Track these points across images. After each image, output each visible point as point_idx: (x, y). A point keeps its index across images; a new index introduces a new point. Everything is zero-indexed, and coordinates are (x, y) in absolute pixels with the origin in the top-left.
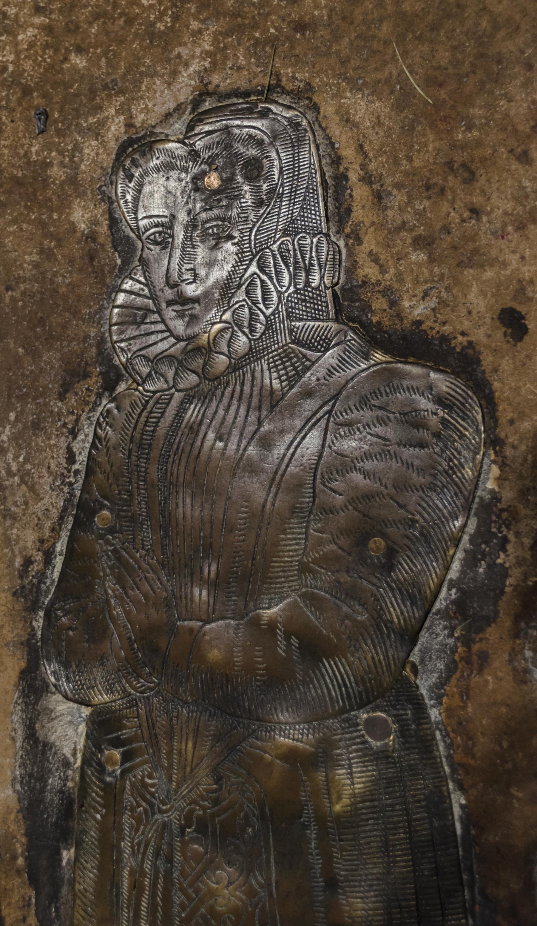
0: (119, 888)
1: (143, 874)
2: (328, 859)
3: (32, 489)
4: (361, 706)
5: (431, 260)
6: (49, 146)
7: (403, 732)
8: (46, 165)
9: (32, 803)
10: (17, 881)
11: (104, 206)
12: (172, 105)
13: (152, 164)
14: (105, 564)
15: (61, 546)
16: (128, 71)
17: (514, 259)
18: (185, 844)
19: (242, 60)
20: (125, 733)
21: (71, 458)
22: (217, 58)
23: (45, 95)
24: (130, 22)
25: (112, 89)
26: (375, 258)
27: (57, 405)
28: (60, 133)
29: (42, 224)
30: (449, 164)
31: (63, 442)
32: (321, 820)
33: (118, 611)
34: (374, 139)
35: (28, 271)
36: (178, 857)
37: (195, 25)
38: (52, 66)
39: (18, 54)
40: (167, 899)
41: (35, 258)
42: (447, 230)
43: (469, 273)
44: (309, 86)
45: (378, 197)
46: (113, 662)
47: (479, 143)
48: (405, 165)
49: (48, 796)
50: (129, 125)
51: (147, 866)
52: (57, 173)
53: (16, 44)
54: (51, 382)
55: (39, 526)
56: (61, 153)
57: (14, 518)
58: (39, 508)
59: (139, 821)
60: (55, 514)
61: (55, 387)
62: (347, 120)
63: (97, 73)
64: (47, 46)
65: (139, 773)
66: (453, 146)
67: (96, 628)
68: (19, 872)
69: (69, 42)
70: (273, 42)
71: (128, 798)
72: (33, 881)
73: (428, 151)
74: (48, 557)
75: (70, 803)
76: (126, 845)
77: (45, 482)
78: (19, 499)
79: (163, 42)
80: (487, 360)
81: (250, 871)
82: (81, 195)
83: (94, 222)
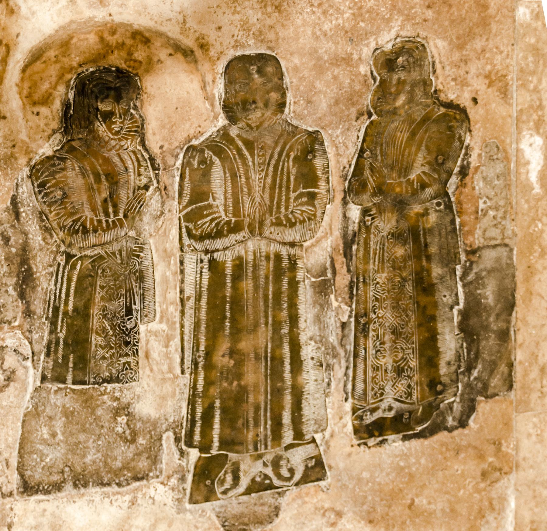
0: (369, 254)
1: (376, 249)
2: (425, 239)
3: (346, 147)
4: (435, 198)
5: (456, 84)
6: (353, 49)
7: (445, 204)
8: (352, 54)
9: (344, 236)
10: (340, 257)
11: (369, 67)
12: (389, 39)
13: (420, 159)
14: (367, 167)
15: (354, 162)
16: (377, 29)
17: (475, 85)
18: (388, 240)
19: (409, 28)
20: (372, 213)
21: (358, 137)
22: (402, 27)
23: (352, 34)
24: (377, 14)
25: (372, 33)
26: (442, 83)
27: (354, 123)
28: (356, 45)
29: (351, 72)
30: (461, 60)
31: (356, 134)
32: (424, 229)
33: (371, 180)
34: (443, 52)
35: (346, 85)
36: (386, 244)
37: (396, 17)
38: (354, 26)
39: (344, 21)
40: (383, 255)
41: (349, 81)
42: (460, 77)
43: (465, 88)
44: (427, 37)
45: (443, 68)
46: (369, 193)
47: (468, 55)
48: (450, 60)
49: (349, 232)
50: (377, 44)
51: (378, 248)
52: (355, 57)
53: (343, 18)
54: (353, 116)
55: (348, 157)
56: (357, 51)
57: (341, 155)
58: (348, 152)
59: (375, 236)
60: (353, 154)
61: (354, 119)
62: (436, 47)
63: (367, 28)
64: (353, 19)
65: (376, 223)
66: (462, 55)
67: (363, 186)
68: (341, 254)
69: (359, 19)
70: (417, 24)
71: (373, 230)
72: (345, 256)
73: (456, 56)
74: (350, 165)
75: (355, 233)
76: (372, 243)
77: (350, 145)
78: (342, 150)
79: (388, 21)
80: (468, 111)
81: (405, 245)
82: (363, 63)
83: (366, 71)
